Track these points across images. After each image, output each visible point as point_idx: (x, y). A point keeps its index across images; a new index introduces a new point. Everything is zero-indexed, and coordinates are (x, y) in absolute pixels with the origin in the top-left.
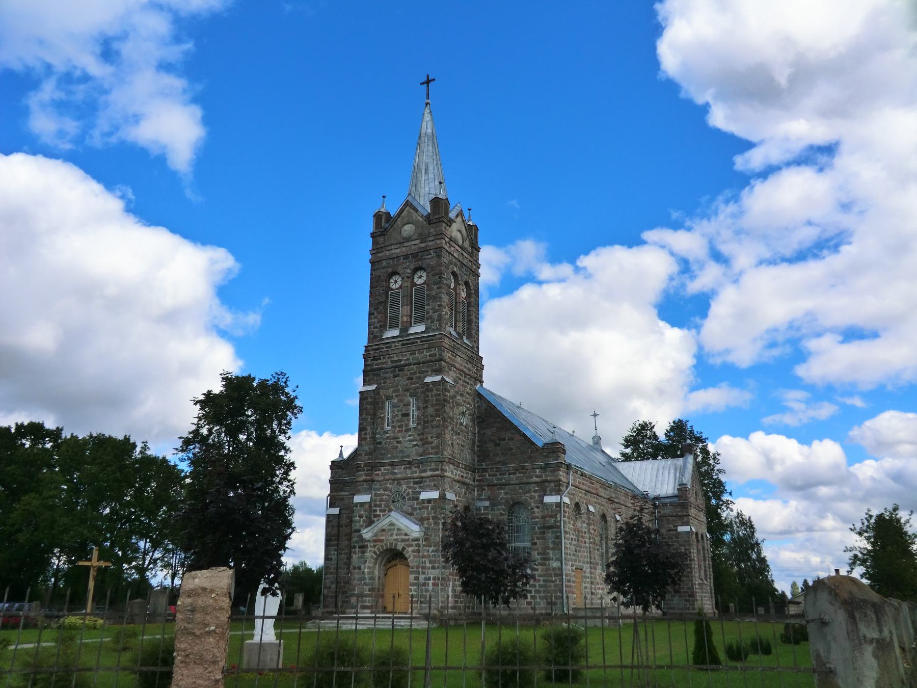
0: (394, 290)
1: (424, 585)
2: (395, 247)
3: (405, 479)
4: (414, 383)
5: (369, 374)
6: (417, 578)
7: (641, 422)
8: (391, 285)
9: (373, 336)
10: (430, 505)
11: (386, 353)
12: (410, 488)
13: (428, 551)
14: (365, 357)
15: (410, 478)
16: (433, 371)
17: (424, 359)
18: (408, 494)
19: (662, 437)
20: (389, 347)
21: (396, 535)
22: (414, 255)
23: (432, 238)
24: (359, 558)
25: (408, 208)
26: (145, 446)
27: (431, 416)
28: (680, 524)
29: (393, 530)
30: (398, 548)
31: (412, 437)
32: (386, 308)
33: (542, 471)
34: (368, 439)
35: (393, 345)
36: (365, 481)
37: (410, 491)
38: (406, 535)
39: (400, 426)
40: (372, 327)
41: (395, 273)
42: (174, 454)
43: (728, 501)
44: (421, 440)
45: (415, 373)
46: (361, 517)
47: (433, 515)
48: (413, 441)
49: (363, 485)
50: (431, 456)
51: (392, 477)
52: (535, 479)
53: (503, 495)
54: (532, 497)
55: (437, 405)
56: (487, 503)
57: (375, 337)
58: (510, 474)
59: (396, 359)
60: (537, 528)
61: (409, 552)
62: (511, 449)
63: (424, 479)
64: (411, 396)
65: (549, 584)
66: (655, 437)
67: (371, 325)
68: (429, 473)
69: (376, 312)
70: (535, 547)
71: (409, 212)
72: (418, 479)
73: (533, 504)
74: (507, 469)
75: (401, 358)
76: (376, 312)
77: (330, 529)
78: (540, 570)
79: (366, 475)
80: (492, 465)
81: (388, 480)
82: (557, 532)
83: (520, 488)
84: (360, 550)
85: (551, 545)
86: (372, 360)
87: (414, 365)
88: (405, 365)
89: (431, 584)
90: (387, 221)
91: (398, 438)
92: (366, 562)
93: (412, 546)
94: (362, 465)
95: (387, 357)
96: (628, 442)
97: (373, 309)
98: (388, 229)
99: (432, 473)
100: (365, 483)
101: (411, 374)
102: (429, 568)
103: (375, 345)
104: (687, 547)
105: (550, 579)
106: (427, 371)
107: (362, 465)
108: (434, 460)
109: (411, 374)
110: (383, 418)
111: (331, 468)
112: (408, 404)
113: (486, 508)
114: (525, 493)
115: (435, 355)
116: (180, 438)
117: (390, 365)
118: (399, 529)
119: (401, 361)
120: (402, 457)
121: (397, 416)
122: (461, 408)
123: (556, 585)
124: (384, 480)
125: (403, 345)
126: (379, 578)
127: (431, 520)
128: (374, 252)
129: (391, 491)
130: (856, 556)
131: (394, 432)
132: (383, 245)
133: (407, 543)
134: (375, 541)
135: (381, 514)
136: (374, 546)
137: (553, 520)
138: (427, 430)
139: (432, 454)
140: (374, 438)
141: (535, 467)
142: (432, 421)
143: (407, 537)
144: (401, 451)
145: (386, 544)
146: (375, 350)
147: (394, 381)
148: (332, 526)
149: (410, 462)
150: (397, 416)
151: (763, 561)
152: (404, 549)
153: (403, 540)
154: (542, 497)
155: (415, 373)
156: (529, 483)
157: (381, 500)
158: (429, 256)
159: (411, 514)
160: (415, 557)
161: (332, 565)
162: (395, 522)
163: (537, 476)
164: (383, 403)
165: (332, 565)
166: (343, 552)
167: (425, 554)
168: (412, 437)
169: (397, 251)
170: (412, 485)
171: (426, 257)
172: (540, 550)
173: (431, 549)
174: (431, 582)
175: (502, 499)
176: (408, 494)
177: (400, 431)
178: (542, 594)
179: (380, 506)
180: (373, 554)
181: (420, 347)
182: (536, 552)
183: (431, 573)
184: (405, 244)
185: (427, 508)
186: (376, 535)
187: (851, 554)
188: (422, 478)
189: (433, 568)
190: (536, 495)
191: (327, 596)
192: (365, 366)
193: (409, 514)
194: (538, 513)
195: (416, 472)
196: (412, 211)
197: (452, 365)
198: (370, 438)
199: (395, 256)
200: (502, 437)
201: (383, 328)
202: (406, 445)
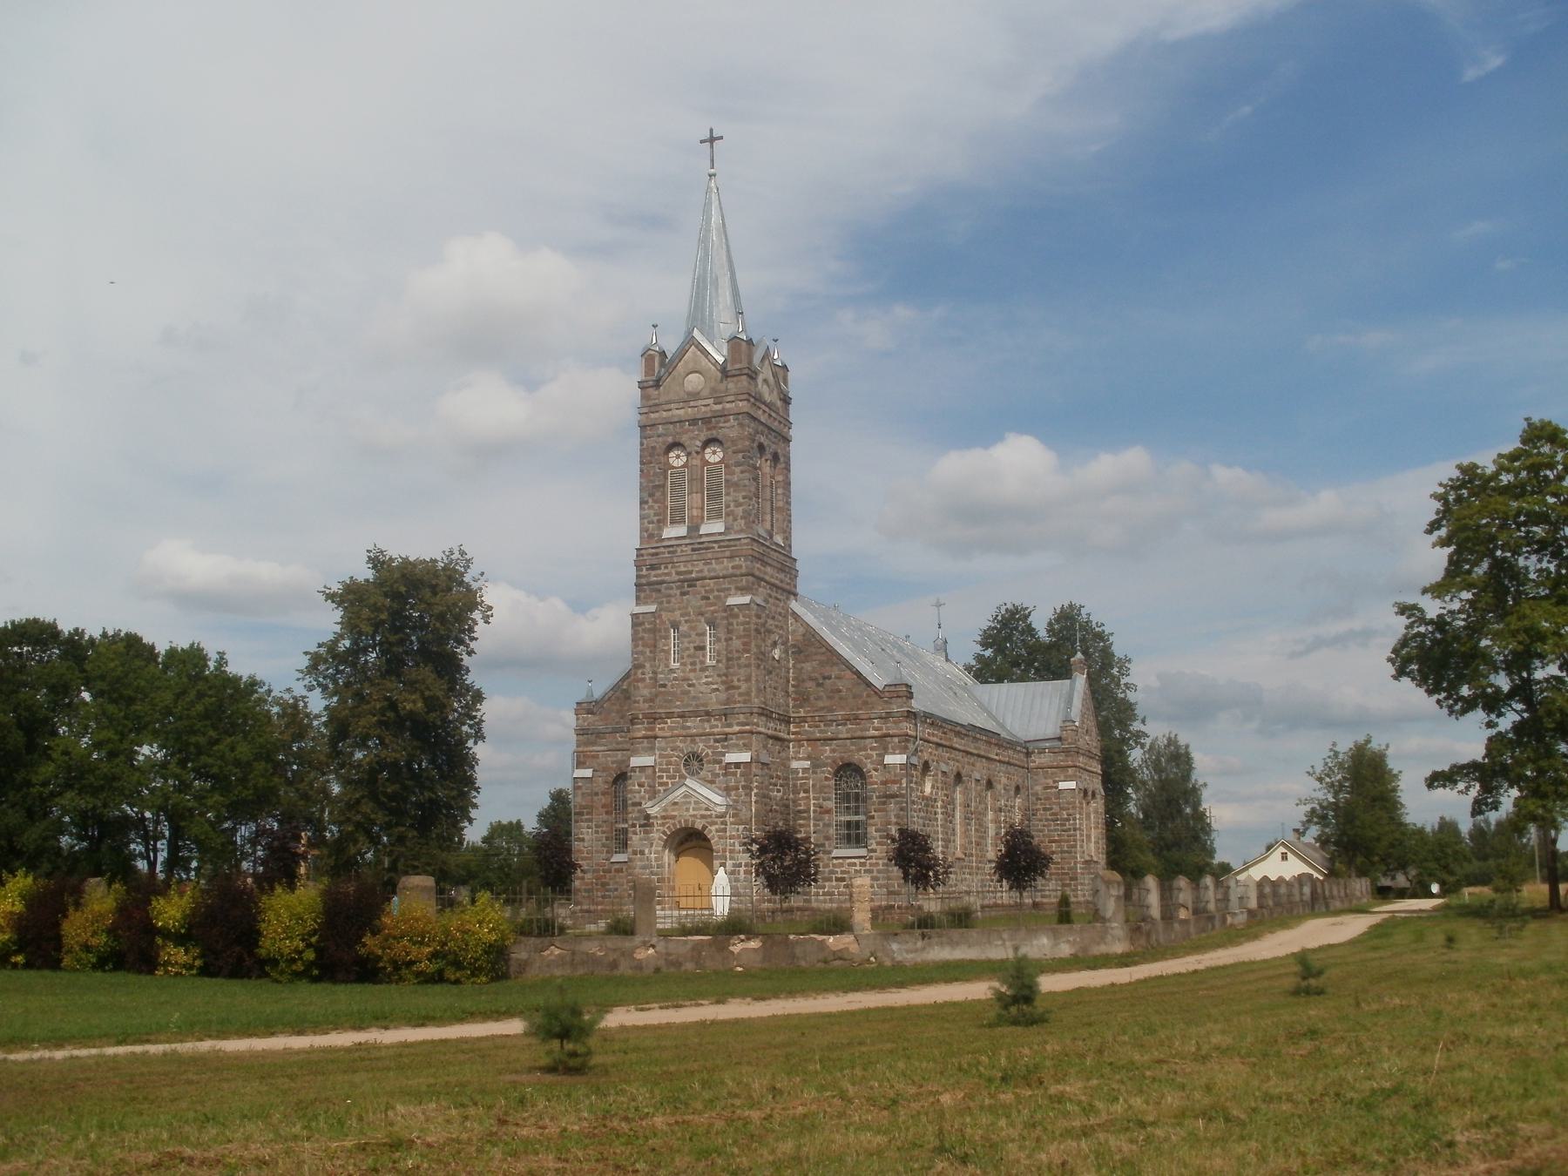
2: (676, 406)
4: (711, 605)
5: (643, 589)
7: (1010, 606)
8: (671, 460)
9: (649, 535)
10: (739, 771)
12: (709, 747)
16: (737, 588)
17: (725, 572)
18: (707, 754)
19: (1042, 633)
21: (694, 809)
22: (706, 421)
24: (641, 839)
26: (222, 658)
27: (738, 651)
28: (1062, 778)
31: (710, 679)
32: (664, 494)
33: (882, 721)
35: (679, 549)
40: (646, 521)
41: (676, 445)
42: (298, 680)
43: (1138, 732)
44: (723, 683)
45: (712, 591)
46: (641, 785)
50: (738, 705)
51: (684, 733)
52: (873, 733)
55: (745, 636)
56: (807, 764)
57: (651, 536)
58: (838, 725)
61: (712, 833)
62: (840, 691)
63: (730, 736)
66: (1030, 630)
68: (736, 728)
69: (650, 500)
70: (871, 821)
74: (834, 718)
76: (650, 500)
79: (646, 729)
82: (902, 802)
83: (852, 744)
84: (642, 829)
86: (647, 570)
88: (698, 580)
89: (742, 872)
90: (662, 364)
91: (688, 680)
92: (652, 845)
93: (716, 823)
95: (670, 566)
96: (988, 639)
98: (664, 378)
100: (646, 741)
101: (706, 592)
104: (1071, 811)
106: (729, 589)
109: (706, 592)
112: (704, 634)
113: (805, 770)
114: (860, 750)
116: (306, 653)
117: (675, 577)
119: (691, 572)
120: (697, 706)
121: (688, 649)
122: (772, 636)
125: (693, 550)
126: (669, 864)
128: (645, 410)
130: (1313, 811)
131: (683, 671)
133: (709, 820)
134: (664, 818)
135: (670, 781)
136: (663, 825)
138: (731, 670)
139: (739, 702)
140: (655, 679)
141: (873, 716)
142: (739, 658)
143: (709, 813)
144: (694, 697)
145: (680, 822)
146: (653, 555)
147: (682, 600)
148: (583, 794)
149: (708, 713)
150: (688, 649)
151: (1200, 817)
152: (704, 827)
153: (703, 817)
154: (882, 756)
155: (712, 591)
157: (669, 763)
158: (727, 425)
159: (712, 782)
160: (720, 837)
164: (667, 631)
168: (710, 679)
169: (681, 412)
170: (712, 743)
174: (742, 869)
175: (827, 758)
176: (707, 754)
177: (694, 671)
179: (667, 771)
181: (719, 555)
184: (692, 404)
185: (734, 774)
186: (665, 810)
187: (1308, 808)
188: (726, 734)
190: (874, 753)
192: (638, 577)
193: (710, 782)
195: (717, 727)
197: (762, 579)
198: (651, 678)
200: (826, 674)
201: (661, 523)
202: (703, 688)
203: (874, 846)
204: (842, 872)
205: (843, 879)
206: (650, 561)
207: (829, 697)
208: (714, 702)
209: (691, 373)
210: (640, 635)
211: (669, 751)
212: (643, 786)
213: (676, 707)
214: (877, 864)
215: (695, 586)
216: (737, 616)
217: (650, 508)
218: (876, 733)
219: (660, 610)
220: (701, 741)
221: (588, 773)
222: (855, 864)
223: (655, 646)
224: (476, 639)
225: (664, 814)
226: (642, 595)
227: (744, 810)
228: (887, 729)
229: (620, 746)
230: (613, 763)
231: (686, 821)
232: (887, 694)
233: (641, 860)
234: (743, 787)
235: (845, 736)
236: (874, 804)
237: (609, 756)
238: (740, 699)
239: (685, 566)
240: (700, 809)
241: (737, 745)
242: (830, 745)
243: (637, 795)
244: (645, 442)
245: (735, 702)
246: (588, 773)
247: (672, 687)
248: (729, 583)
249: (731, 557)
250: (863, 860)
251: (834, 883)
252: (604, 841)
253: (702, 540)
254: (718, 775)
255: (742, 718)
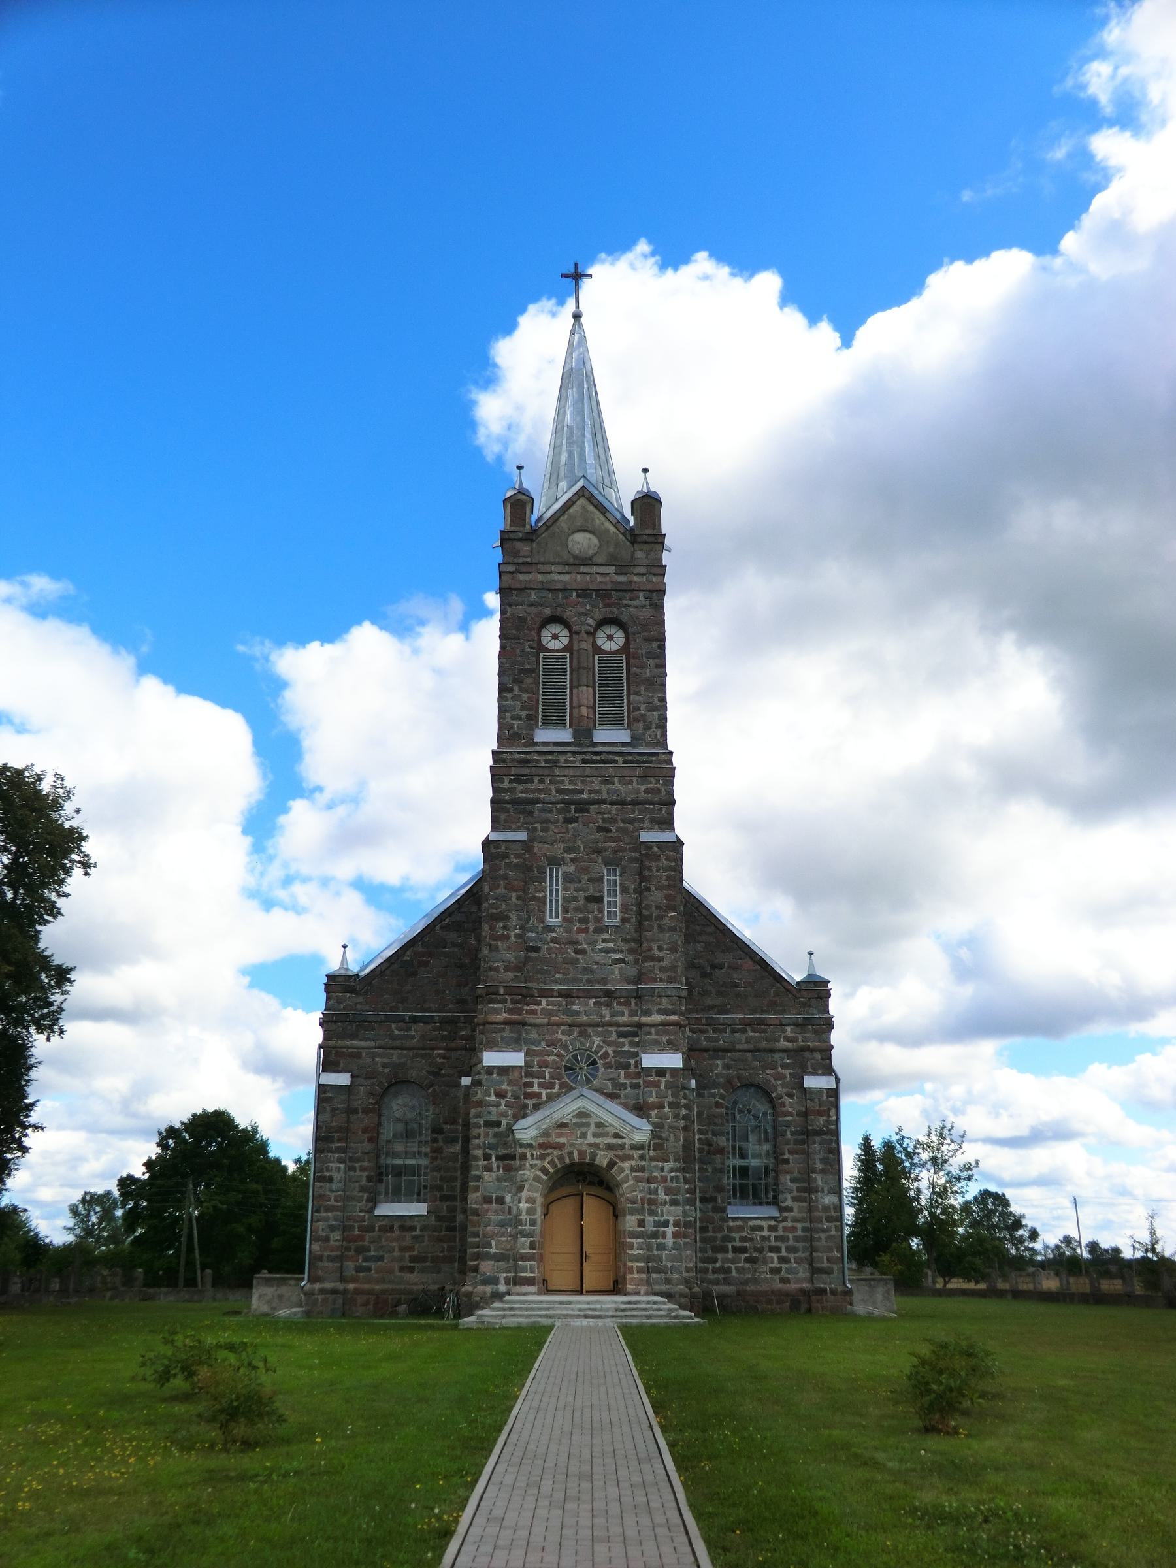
0: (606, 652)
1: (655, 1235)
2: (560, 568)
3: (598, 1026)
6: (641, 1223)
10: (663, 1080)
11: (547, 772)
12: (609, 1044)
13: (662, 1169)
14: (496, 775)
15: (610, 1024)
16: (653, 821)
18: (606, 1055)
20: (556, 762)
21: (595, 1135)
22: (603, 594)
23: (643, 570)
24: (498, 1179)
25: (582, 501)
27: (658, 907)
29: (588, 1125)
30: (597, 1161)
31: (611, 945)
33: (798, 1030)
34: (513, 939)
35: (562, 759)
36: (507, 1023)
37: (610, 1050)
38: (617, 1136)
39: (584, 921)
40: (508, 715)
44: (631, 951)
45: (614, 820)
46: (501, 1095)
47: (670, 1099)
48: (614, 951)
49: (503, 1030)
52: (784, 1044)
53: (720, 1068)
54: (779, 1077)
58: (733, 1031)
59: (568, 786)
60: (788, 1133)
62: (736, 986)
64: (606, 864)
65: (816, 1236)
67: (506, 711)
68: (658, 1018)
69: (516, 688)
70: (785, 1167)
71: (584, 508)
72: (628, 1028)
73: (780, 1089)
75: (580, 786)
76: (516, 688)
77: (326, 1117)
78: (795, 1210)
79: (509, 1011)
80: (697, 1012)
81: (558, 1025)
82: (831, 1141)
85: (819, 1166)
86: (511, 781)
87: (612, 803)
89: (669, 1235)
91: (576, 943)
92: (520, 1189)
93: (631, 1158)
94: (502, 991)
95: (548, 780)
97: (507, 680)
99: (663, 1017)
100: (508, 1028)
101: (604, 820)
102: (665, 1203)
103: (519, 753)
105: (820, 1226)
106: (642, 821)
107: (502, 991)
108: (669, 993)
109: (604, 820)
110: (542, 901)
111: (328, 989)
112: (601, 879)
115: (658, 791)
117: (554, 796)
118: (599, 1125)
119: (581, 792)
120: (589, 981)
121: (575, 899)
123: (827, 1239)
124: (549, 1024)
125: (584, 761)
127: (667, 1109)
129: (565, 1047)
131: (569, 931)
132: (528, 560)
133: (620, 1152)
135: (544, 1092)
136: (542, 1157)
137: (821, 1120)
139: (661, 980)
142: (660, 918)
143: (619, 1141)
144: (585, 969)
145: (570, 1154)
147: (567, 828)
148: (333, 1110)
149: (608, 994)
150: (575, 899)
153: (610, 1147)
155: (614, 820)
156: (772, 1051)
160: (638, 1180)
161: (331, 1191)
162: (591, 1107)
163: (788, 1039)
165: (331, 1191)
166: (357, 1165)
167: (655, 1174)
168: (611, 945)
169: (566, 578)
170: (614, 1037)
171: (630, 603)
172: (796, 1174)
173: (668, 1166)
174: (670, 1230)
176: (606, 1055)
178: (800, 1254)
179: (541, 1076)
180: (539, 1173)
181: (625, 773)
182: (788, 1177)
183: (669, 1213)
184: (582, 569)
185: (657, 1085)
186: (546, 1134)
188: (639, 1026)
189: (674, 1202)
190: (787, 1072)
191: (320, 1258)
194: (791, 1105)
195: (622, 1014)
196: (591, 508)
199: (559, 586)
200: (716, 961)
203: (789, 1203)
204: (743, 1239)
205: (743, 1250)
206: (515, 768)
207: (720, 993)
208: (617, 977)
209: (579, 531)
210: (502, 872)
211: (543, 1046)
212: (504, 1097)
213: (556, 982)
214: (794, 1229)
215: (588, 811)
216: (658, 858)
217: (515, 698)
218: (790, 1045)
219: (531, 840)
220: (598, 1034)
221: (343, 1079)
222: (761, 1228)
223: (524, 891)
224: (66, 895)
225: (542, 1140)
226: (503, 816)
227: (672, 1139)
228: (805, 1040)
229: (398, 1043)
230: (384, 1066)
231: (581, 1153)
232: (805, 994)
233: (497, 1212)
234: (671, 1105)
235: (746, 1046)
236: (787, 1143)
237: (379, 1056)
238: (662, 975)
239: (571, 782)
240: (605, 1135)
241: (656, 1043)
242: (722, 1058)
243: (493, 1110)
244: (509, 609)
245: (655, 980)
246: (343, 1079)
247: (549, 951)
248: (640, 812)
249: (644, 777)
250: (773, 1223)
251: (730, 1255)
252: (364, 1182)
253: (597, 750)
254: (624, 1086)
255: (666, 1004)
